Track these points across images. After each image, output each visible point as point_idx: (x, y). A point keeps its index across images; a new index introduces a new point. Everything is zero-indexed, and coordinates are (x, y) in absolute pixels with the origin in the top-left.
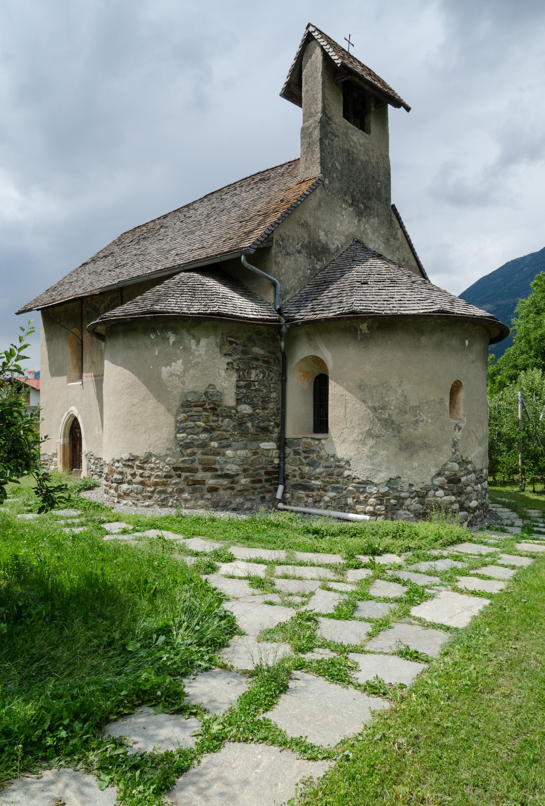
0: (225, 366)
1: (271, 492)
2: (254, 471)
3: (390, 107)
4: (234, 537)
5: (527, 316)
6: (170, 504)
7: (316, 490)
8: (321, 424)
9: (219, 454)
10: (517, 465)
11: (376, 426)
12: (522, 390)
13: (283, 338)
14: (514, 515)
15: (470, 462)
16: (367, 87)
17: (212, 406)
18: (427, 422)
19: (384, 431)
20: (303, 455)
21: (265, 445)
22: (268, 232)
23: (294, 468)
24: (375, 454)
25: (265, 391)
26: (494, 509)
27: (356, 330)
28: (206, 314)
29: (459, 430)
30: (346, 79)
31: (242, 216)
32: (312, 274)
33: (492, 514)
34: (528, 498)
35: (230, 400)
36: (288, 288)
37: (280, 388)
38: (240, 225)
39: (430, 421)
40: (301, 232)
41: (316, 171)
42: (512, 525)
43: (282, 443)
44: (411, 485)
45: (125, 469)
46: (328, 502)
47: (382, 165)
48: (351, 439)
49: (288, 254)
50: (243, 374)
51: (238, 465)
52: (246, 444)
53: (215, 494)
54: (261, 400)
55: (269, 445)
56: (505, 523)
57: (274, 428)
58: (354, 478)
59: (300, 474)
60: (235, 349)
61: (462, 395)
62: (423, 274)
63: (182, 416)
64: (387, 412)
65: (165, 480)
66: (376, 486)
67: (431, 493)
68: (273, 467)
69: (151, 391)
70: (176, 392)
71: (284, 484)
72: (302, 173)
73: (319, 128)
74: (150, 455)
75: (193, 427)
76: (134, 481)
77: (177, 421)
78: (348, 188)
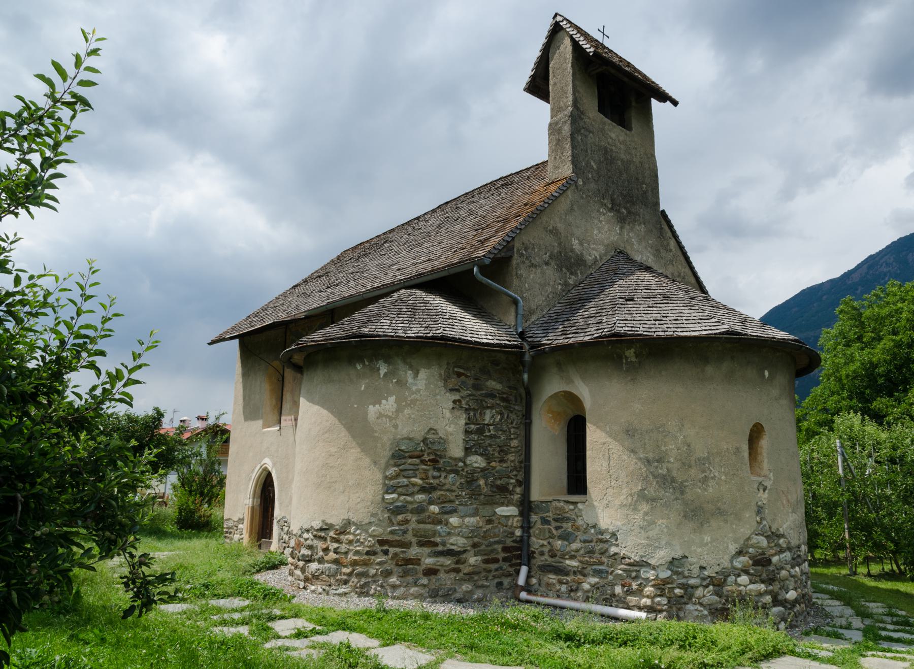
0: (451, 405)
1: (510, 575)
2: (487, 546)
3: (654, 102)
4: (453, 644)
5: (835, 349)
6: (372, 592)
7: (571, 573)
8: (577, 482)
9: (440, 522)
10: (844, 538)
11: (651, 485)
12: (840, 437)
13: (526, 369)
14: (849, 611)
15: (783, 536)
16: (626, 79)
19: (661, 493)
20: (554, 524)
21: (502, 511)
22: (507, 238)
23: (541, 542)
24: (651, 523)
25: (503, 438)
26: (819, 602)
27: (620, 357)
28: (426, 338)
29: (764, 490)
30: (600, 70)
33: (818, 608)
34: (863, 585)
35: (456, 450)
36: (533, 307)
37: (523, 433)
38: (475, 233)
39: (723, 478)
40: (549, 239)
41: (567, 170)
42: (848, 627)
43: (526, 507)
44: (702, 568)
45: (315, 541)
46: (588, 591)
47: (647, 166)
48: (617, 502)
49: (533, 265)
50: (475, 415)
51: (467, 538)
52: (477, 508)
54: (498, 449)
56: (838, 624)
57: (515, 487)
58: (624, 558)
59: (549, 551)
60: (463, 383)
61: (764, 443)
62: (702, 289)
63: (392, 471)
64: (665, 465)
65: (366, 557)
66: (654, 569)
67: (731, 579)
68: (514, 541)
69: (354, 437)
70: (385, 439)
71: (528, 565)
72: (551, 174)
73: (569, 122)
74: (348, 523)
75: (407, 486)
76: (326, 558)
77: (386, 477)
78: (607, 190)
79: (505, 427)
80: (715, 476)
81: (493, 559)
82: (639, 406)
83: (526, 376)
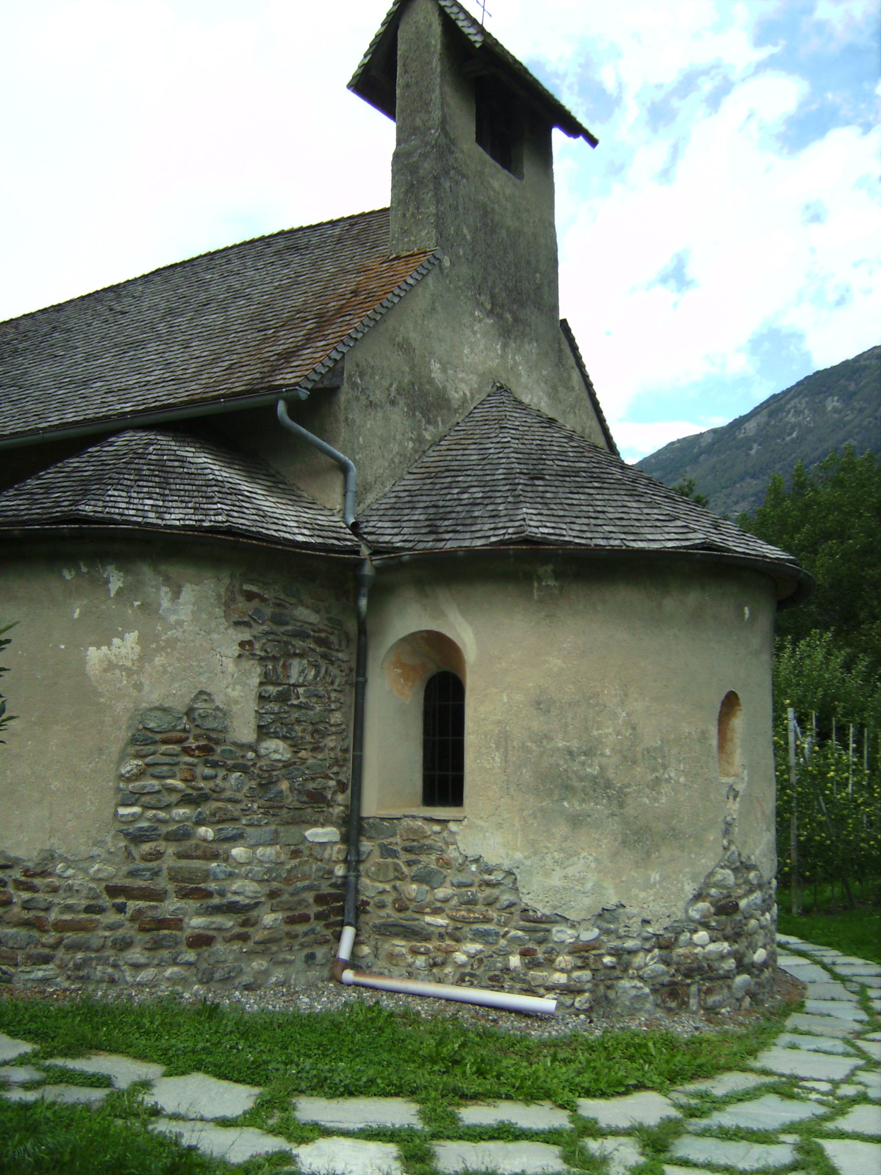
0: (236, 650)
1: (327, 942)
2: (292, 895)
7: (434, 937)
8: (443, 780)
9: (215, 856)
13: (365, 590)
15: (753, 867)
17: (202, 743)
18: (677, 782)
20: (405, 856)
23: (381, 886)
25: (318, 708)
28: (201, 529)
29: (735, 797)
31: (258, 316)
32: (416, 452)
36: (370, 479)
39: (682, 780)
43: (354, 827)
44: (646, 922)
46: (463, 965)
49: (371, 405)
51: (260, 881)
52: (276, 832)
53: (206, 951)
54: (310, 728)
55: (323, 834)
57: (335, 793)
59: (395, 901)
63: (131, 766)
64: (596, 760)
66: (573, 926)
67: (685, 937)
68: (333, 885)
70: (119, 707)
75: (159, 792)
78: (485, 279)
79: (321, 690)
80: (670, 778)
81: (300, 915)
82: (559, 662)
83: (363, 602)
